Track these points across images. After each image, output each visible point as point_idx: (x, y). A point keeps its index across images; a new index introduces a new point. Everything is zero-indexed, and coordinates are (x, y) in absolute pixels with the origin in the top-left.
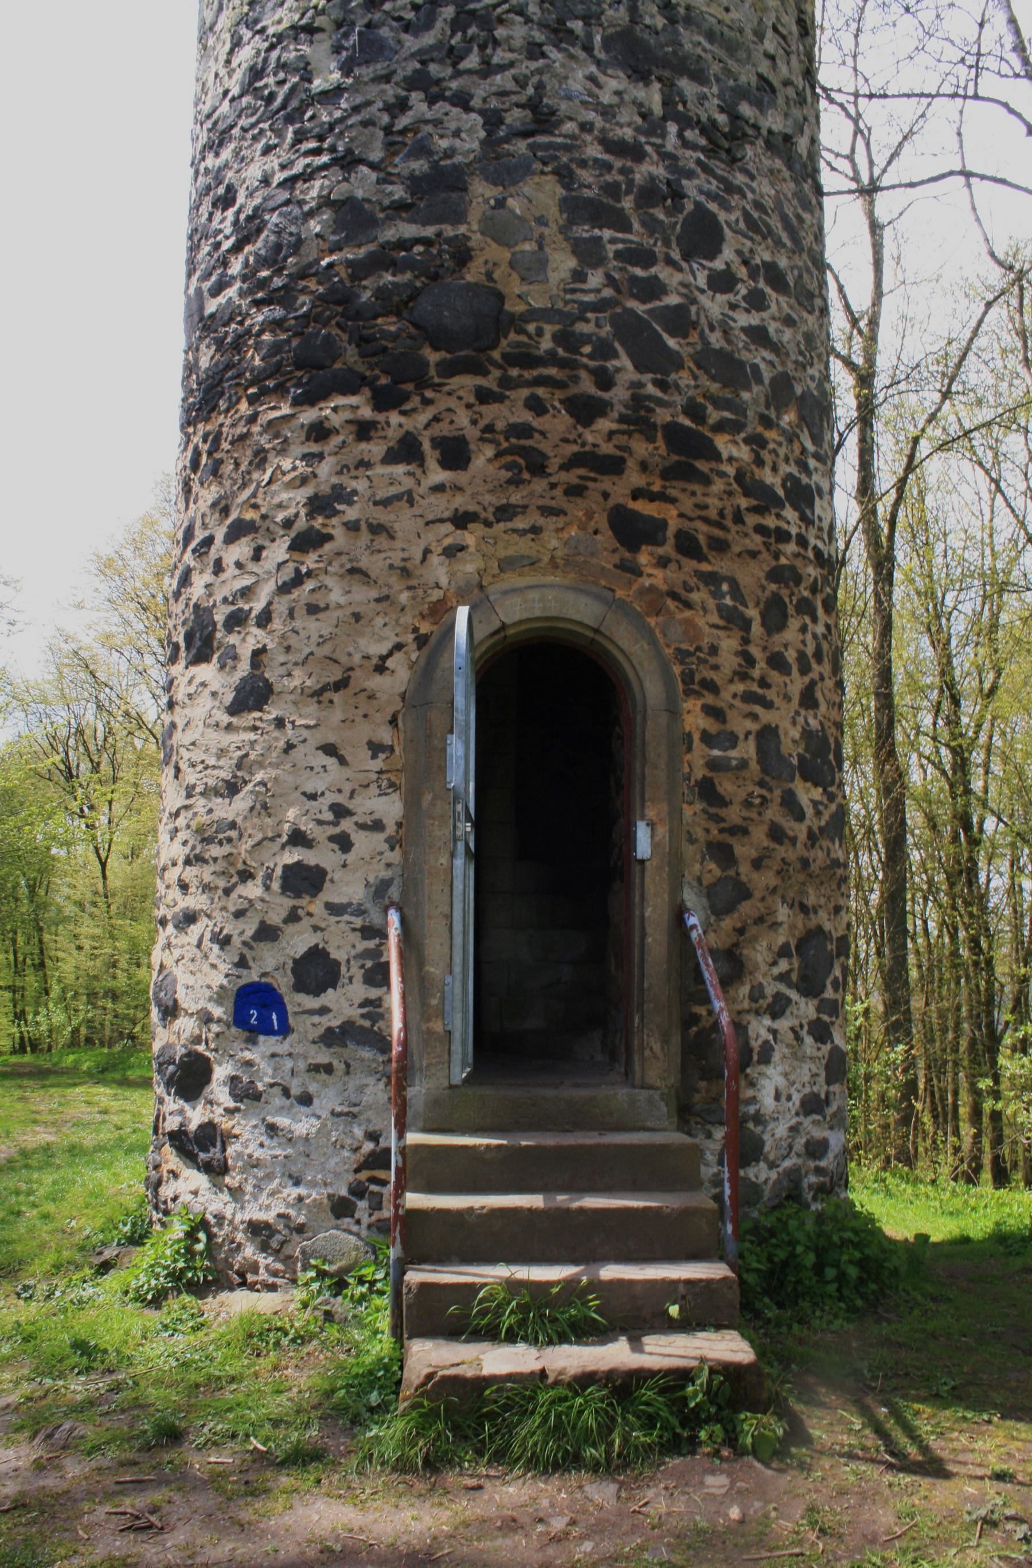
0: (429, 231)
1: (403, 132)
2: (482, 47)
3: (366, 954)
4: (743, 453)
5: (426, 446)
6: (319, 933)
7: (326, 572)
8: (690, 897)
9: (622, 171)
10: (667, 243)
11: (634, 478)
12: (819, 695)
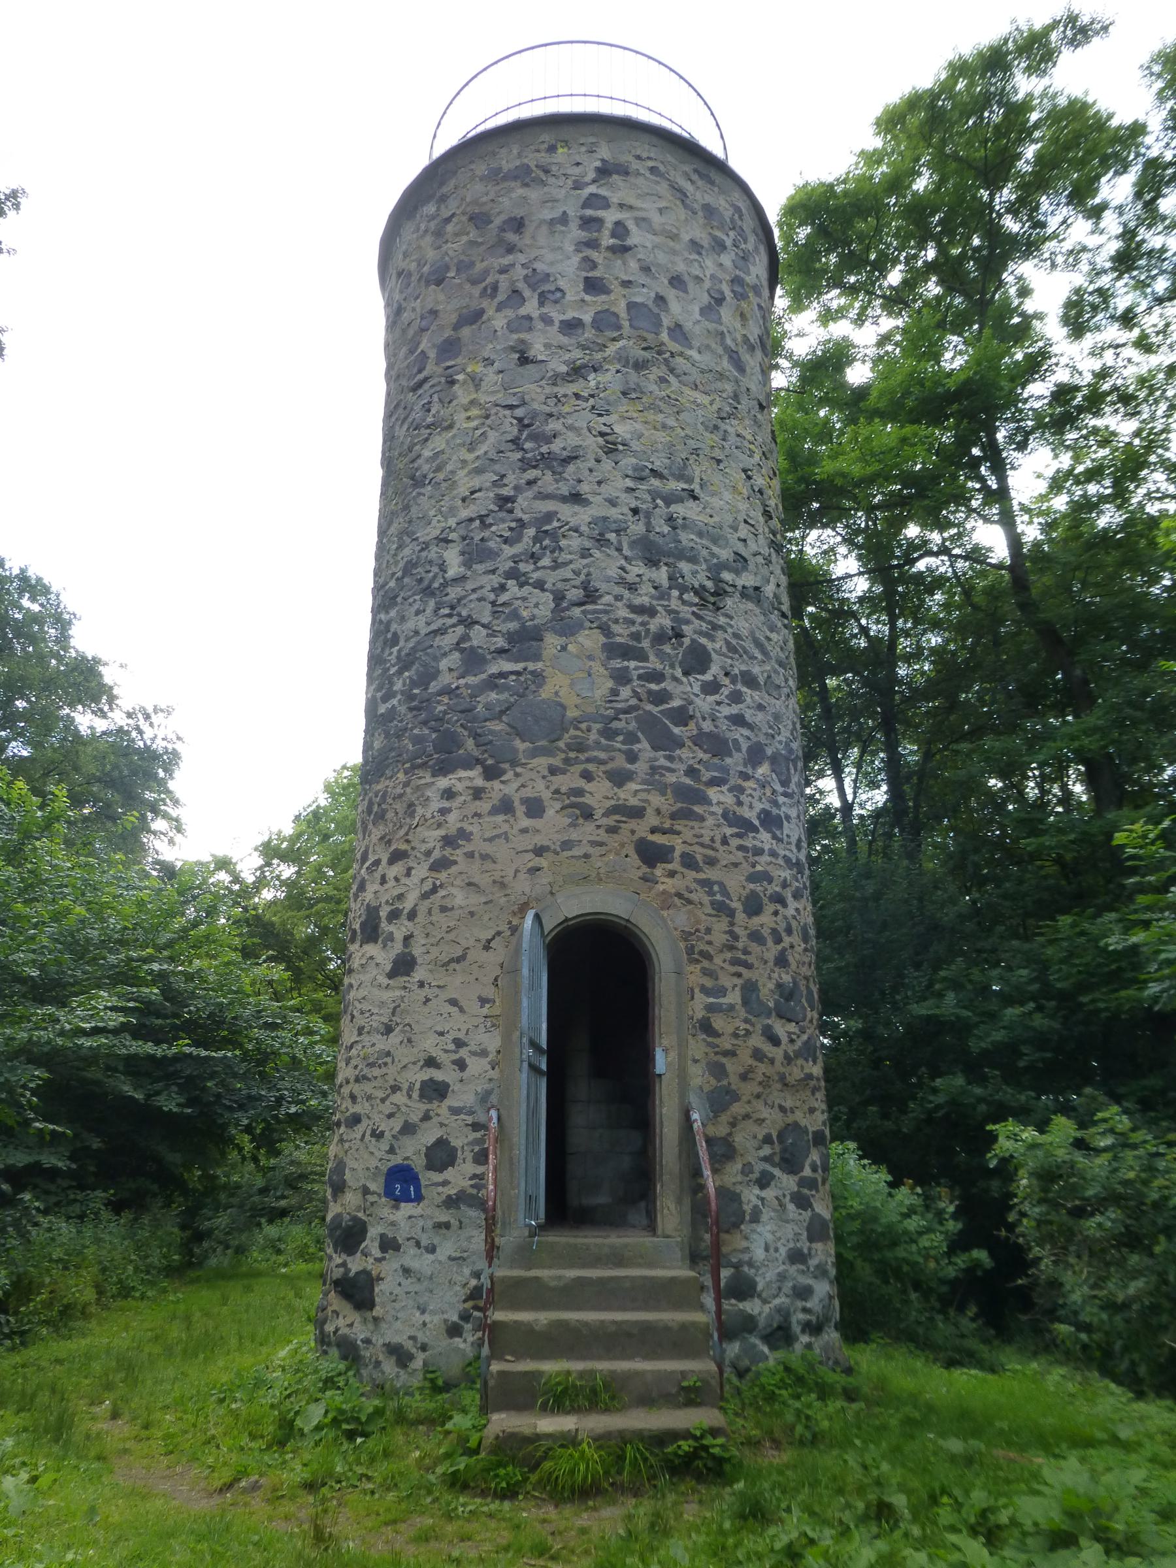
0: (519, 667)
1: (503, 604)
2: (552, 552)
3: (476, 1142)
4: (729, 799)
5: (517, 804)
8: (694, 1099)
9: (643, 624)
10: (672, 666)
11: (652, 820)
12: (790, 958)
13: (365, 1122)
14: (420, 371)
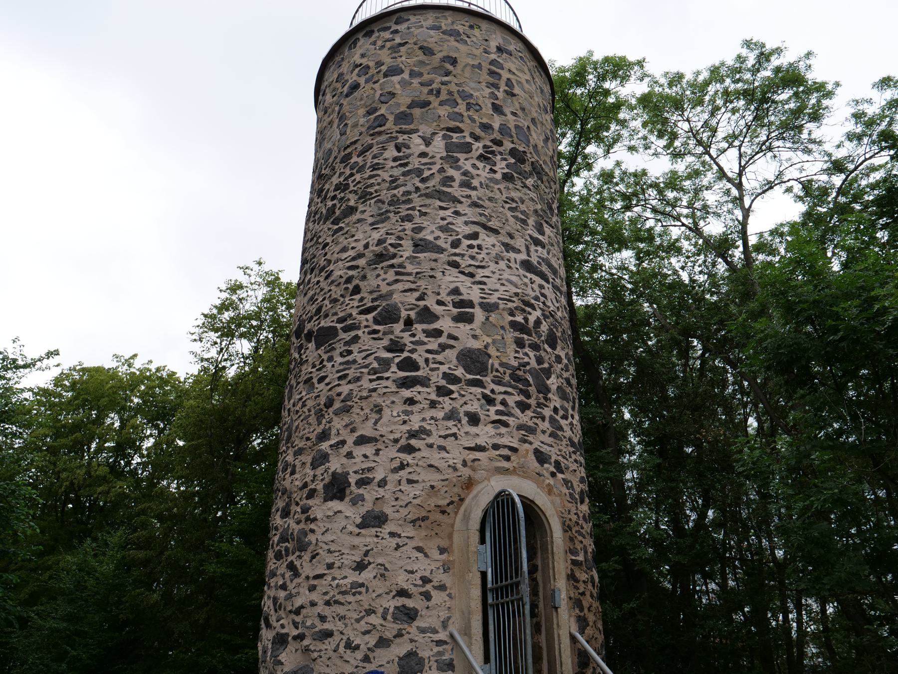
5: (461, 415)
6: (413, 643)
7: (417, 465)
13: (337, 637)
14: (381, 126)
